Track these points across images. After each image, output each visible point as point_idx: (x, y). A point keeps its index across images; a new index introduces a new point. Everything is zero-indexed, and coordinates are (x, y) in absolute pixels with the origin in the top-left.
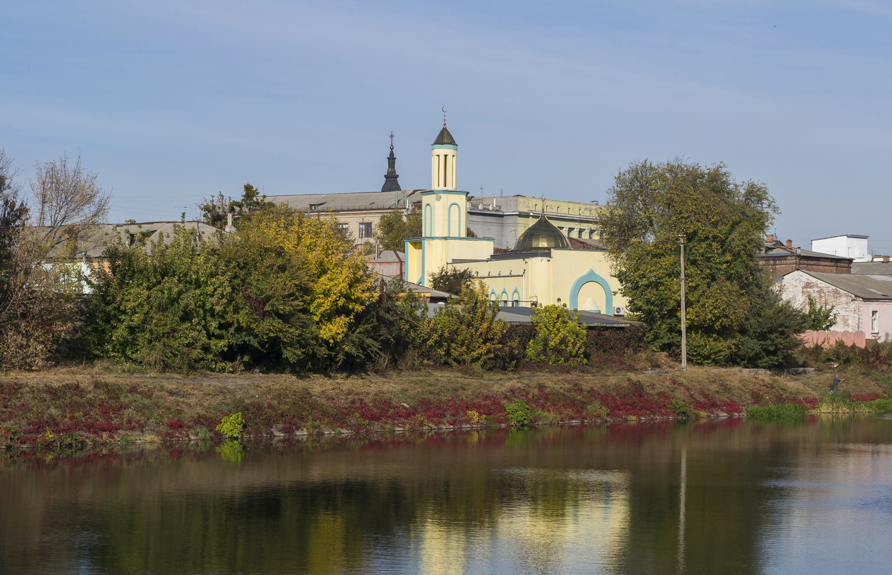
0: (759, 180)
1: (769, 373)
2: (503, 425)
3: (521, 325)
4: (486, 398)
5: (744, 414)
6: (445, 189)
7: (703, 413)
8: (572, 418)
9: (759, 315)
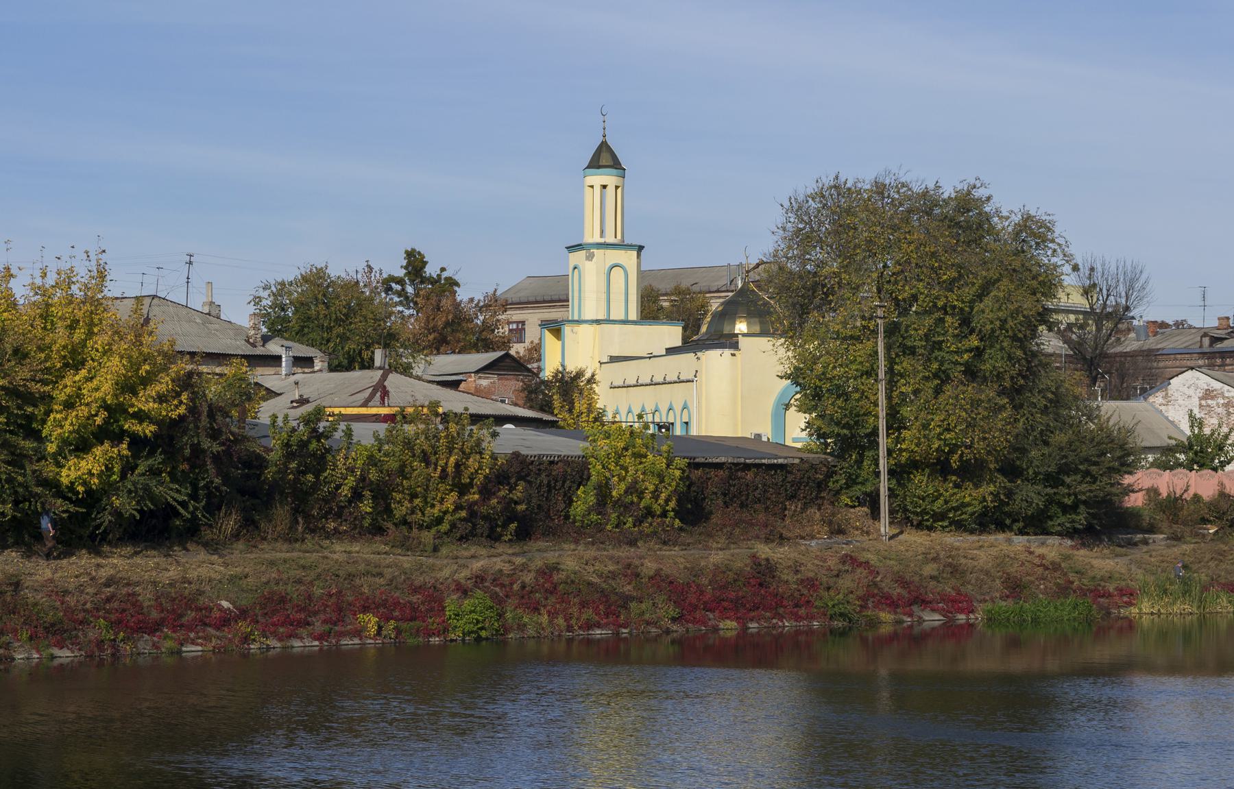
0: (1039, 208)
1: (1069, 542)
2: (435, 640)
3: (566, 461)
4: (416, 590)
5: (978, 617)
6: (602, 241)
7: (886, 616)
8: (589, 626)
9: (1046, 443)
